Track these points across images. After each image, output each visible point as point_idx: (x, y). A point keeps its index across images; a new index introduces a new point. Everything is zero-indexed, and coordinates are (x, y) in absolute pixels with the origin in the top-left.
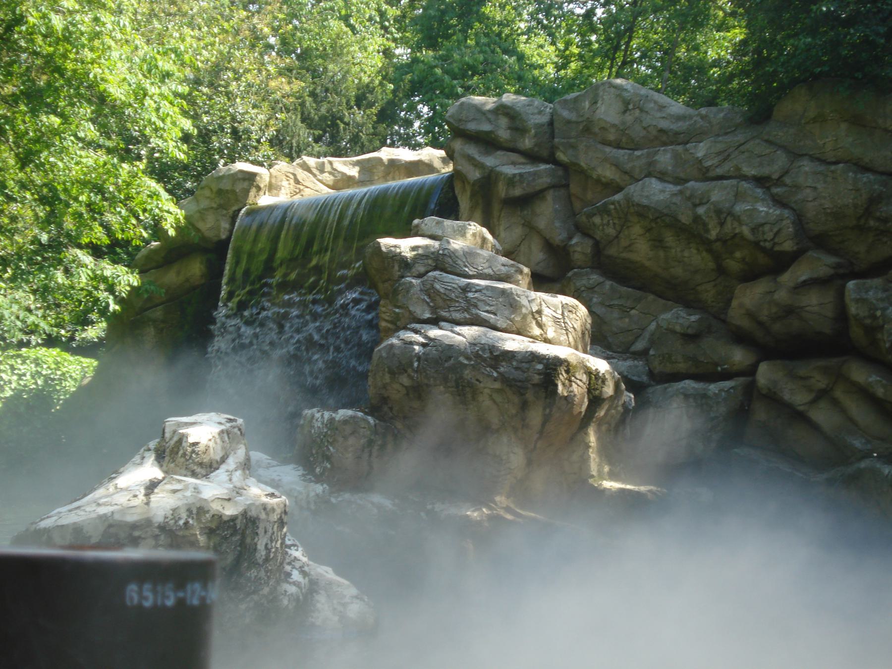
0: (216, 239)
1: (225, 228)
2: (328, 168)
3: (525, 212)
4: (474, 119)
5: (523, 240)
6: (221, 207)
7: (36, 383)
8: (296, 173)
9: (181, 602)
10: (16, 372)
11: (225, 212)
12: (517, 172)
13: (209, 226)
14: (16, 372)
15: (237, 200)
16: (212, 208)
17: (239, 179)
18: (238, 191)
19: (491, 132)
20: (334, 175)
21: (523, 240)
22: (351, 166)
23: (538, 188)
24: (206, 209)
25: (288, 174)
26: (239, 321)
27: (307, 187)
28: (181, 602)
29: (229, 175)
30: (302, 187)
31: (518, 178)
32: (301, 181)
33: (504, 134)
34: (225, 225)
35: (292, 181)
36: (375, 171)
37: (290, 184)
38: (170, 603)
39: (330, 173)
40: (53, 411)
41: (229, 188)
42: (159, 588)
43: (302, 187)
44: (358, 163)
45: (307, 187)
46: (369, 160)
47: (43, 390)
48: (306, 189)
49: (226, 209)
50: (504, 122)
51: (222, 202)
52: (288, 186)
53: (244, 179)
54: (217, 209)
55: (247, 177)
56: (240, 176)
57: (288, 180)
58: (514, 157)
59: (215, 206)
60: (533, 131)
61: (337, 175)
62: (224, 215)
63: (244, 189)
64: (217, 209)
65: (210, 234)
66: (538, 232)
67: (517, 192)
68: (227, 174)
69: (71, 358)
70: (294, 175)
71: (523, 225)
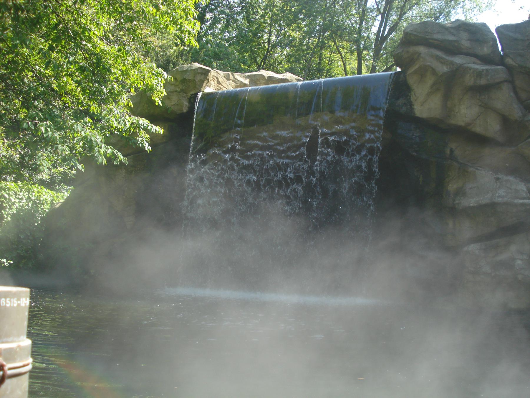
0: (179, 112)
1: (186, 105)
2: (231, 77)
3: (483, 97)
4: (438, 32)
5: (479, 116)
6: (182, 91)
7: (28, 205)
8: (218, 77)
9: (19, 305)
10: (17, 196)
11: (185, 95)
12: (485, 68)
13: (173, 103)
14: (17, 196)
15: (195, 87)
16: (176, 91)
17: (199, 73)
18: (197, 81)
19: (455, 41)
20: (235, 82)
21: (479, 116)
22: (245, 78)
23: (497, 81)
24: (172, 92)
25: (214, 77)
26: (193, 167)
27: (224, 87)
28: (19, 305)
29: (191, 70)
30: (221, 87)
31: (485, 72)
32: (221, 83)
33: (465, 43)
34: (186, 103)
35: (216, 82)
36: (258, 82)
37: (215, 83)
38: (15, 305)
39: (233, 81)
40: (36, 224)
41: (191, 78)
42: (12, 300)
43: (221, 87)
44: (248, 77)
45: (224, 87)
46: (255, 75)
47: (31, 210)
48: (223, 88)
49: (186, 94)
50: (464, 35)
51: (184, 88)
52: (214, 85)
53: (202, 74)
54: (180, 92)
55: (204, 72)
56: (199, 71)
57: (214, 81)
58: (473, 59)
59: (178, 90)
60: (491, 43)
61: (237, 82)
62: (184, 97)
63: (201, 80)
64: (180, 92)
65: (175, 109)
66: (495, 111)
67: (483, 82)
68: (190, 69)
69: (45, 190)
70: (217, 78)
71: (480, 106)
